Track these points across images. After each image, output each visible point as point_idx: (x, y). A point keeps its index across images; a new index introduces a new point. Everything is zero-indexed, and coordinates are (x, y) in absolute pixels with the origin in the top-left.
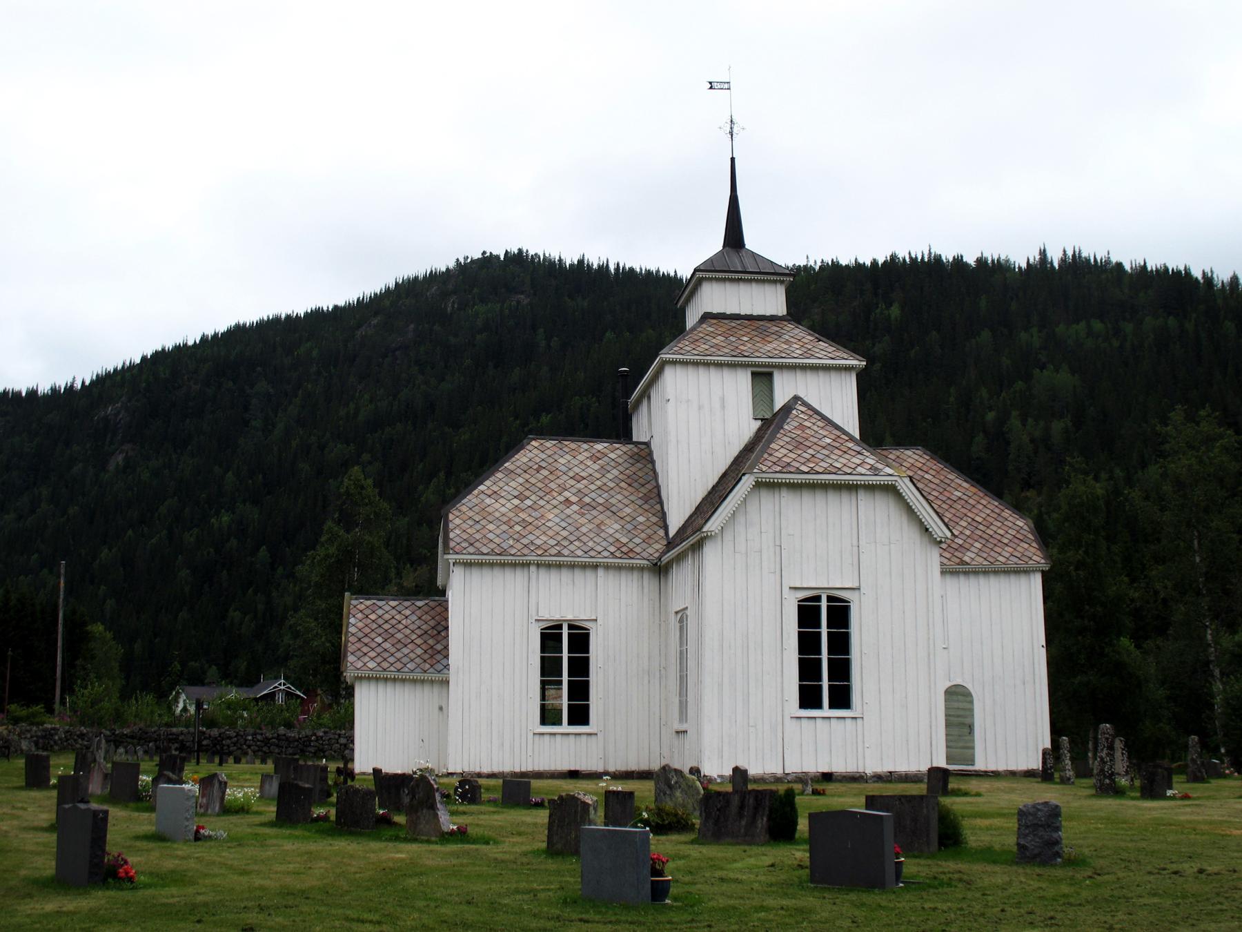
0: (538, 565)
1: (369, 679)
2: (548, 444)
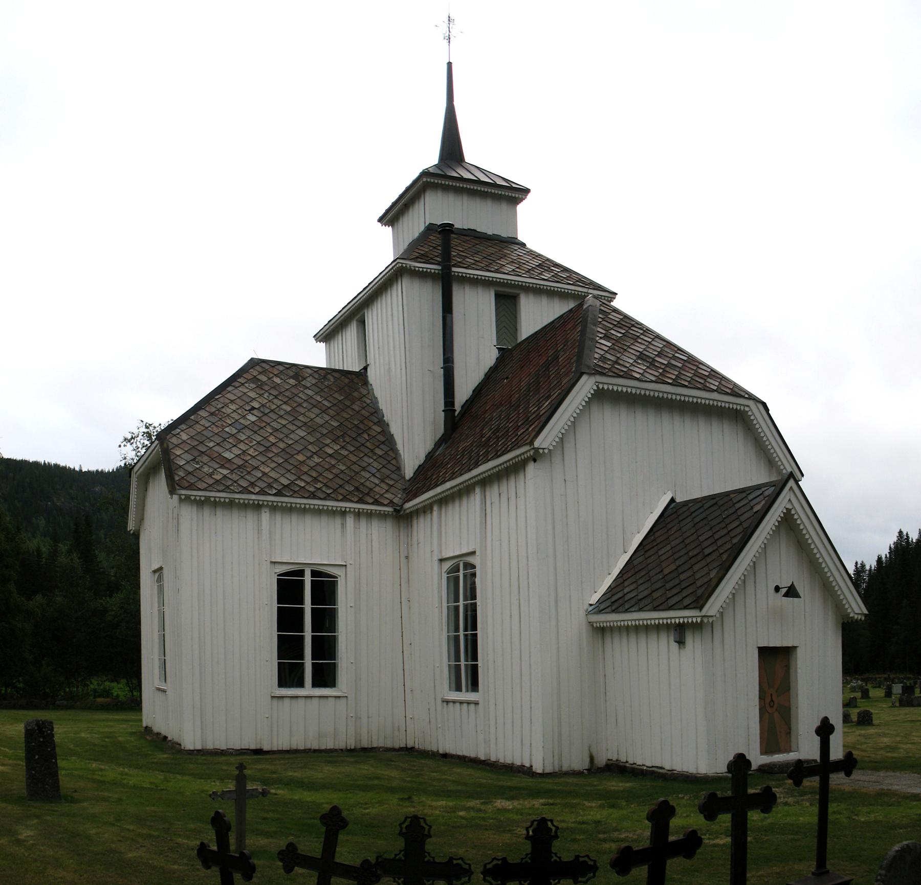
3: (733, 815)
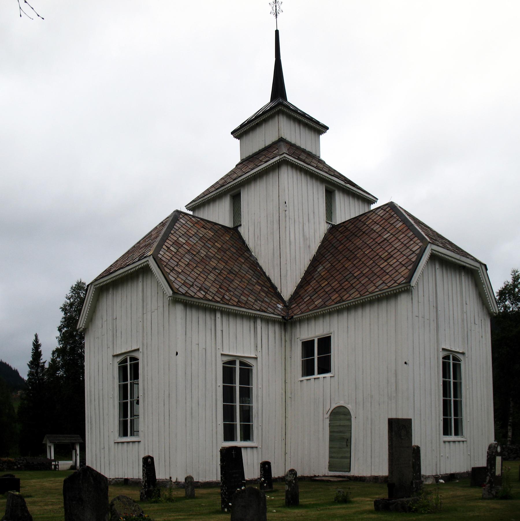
3: (244, 479)
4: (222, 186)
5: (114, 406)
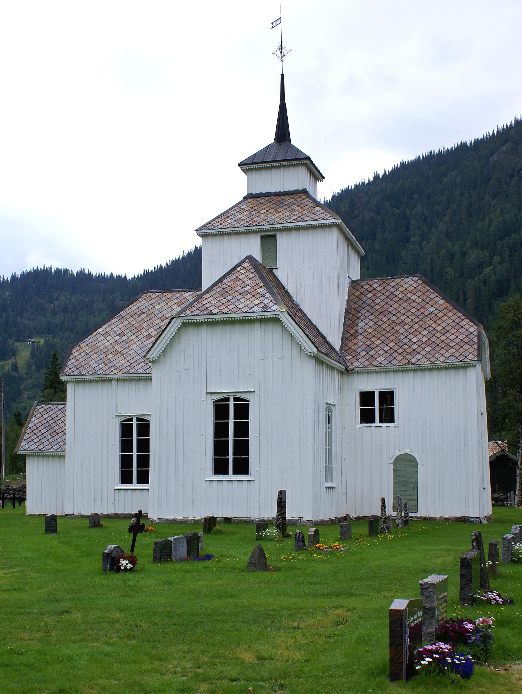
0: (118, 380)
1: (34, 456)
2: (154, 296)
4: (388, 279)
5: (336, 456)
